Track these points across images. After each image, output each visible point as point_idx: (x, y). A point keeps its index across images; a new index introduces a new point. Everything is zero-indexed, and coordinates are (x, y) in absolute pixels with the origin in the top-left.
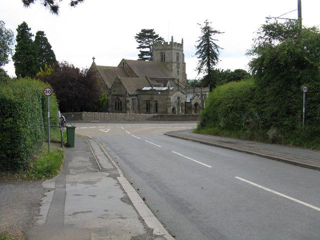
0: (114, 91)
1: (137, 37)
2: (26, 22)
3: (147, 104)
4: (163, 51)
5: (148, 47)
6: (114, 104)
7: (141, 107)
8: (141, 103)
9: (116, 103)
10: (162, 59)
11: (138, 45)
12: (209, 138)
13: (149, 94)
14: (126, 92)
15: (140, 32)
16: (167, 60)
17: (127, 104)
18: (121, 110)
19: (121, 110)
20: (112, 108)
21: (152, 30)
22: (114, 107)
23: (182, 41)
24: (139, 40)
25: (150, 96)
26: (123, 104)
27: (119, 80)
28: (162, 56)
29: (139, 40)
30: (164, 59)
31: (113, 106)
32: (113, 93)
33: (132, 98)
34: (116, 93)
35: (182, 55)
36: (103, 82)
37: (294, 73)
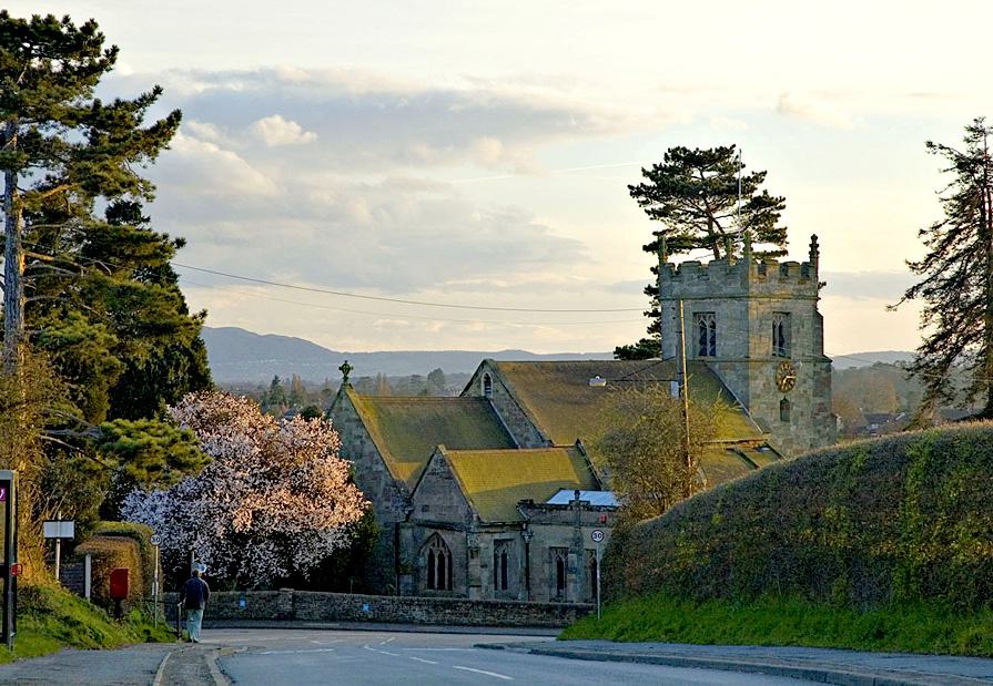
0: (425, 509)
1: (636, 192)
2: (53, 14)
3: (560, 564)
4: (708, 306)
5: (703, 243)
6: (423, 561)
7: (536, 576)
8: (536, 560)
9: (431, 556)
10: (703, 341)
11: (648, 229)
12: (676, 676)
13: (567, 523)
14: (470, 514)
15: (660, 161)
16: (725, 346)
17: (472, 562)
18: (450, 588)
19: (450, 588)
20: (417, 579)
21: (724, 152)
22: (424, 574)
23: (814, 246)
24: (658, 206)
25: (569, 531)
26: (456, 560)
27: (442, 461)
28: (703, 329)
29: (658, 206)
30: (713, 343)
31: (417, 570)
32: (419, 516)
33: (497, 536)
34: (430, 516)
35: (808, 325)
36: (381, 468)
37: (493, 497)
